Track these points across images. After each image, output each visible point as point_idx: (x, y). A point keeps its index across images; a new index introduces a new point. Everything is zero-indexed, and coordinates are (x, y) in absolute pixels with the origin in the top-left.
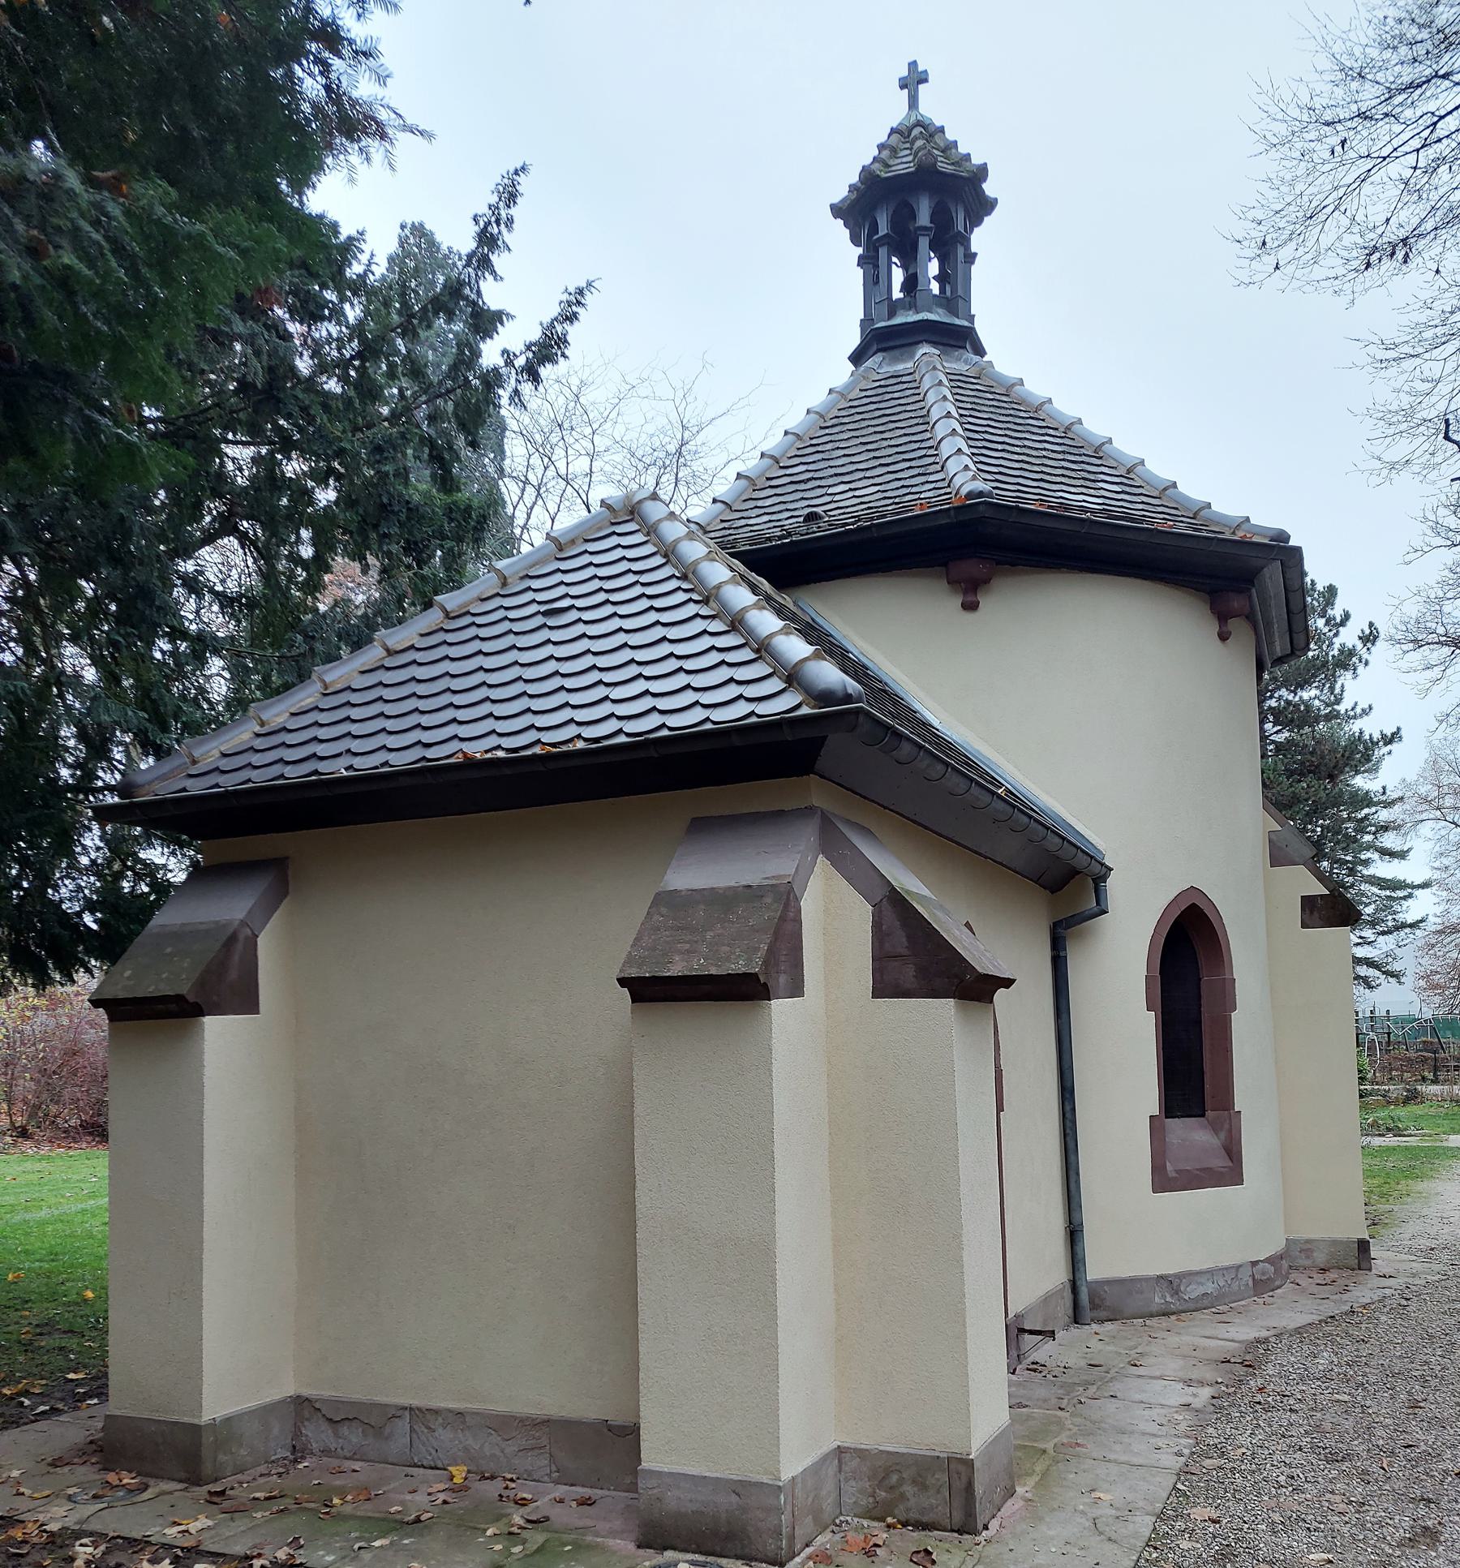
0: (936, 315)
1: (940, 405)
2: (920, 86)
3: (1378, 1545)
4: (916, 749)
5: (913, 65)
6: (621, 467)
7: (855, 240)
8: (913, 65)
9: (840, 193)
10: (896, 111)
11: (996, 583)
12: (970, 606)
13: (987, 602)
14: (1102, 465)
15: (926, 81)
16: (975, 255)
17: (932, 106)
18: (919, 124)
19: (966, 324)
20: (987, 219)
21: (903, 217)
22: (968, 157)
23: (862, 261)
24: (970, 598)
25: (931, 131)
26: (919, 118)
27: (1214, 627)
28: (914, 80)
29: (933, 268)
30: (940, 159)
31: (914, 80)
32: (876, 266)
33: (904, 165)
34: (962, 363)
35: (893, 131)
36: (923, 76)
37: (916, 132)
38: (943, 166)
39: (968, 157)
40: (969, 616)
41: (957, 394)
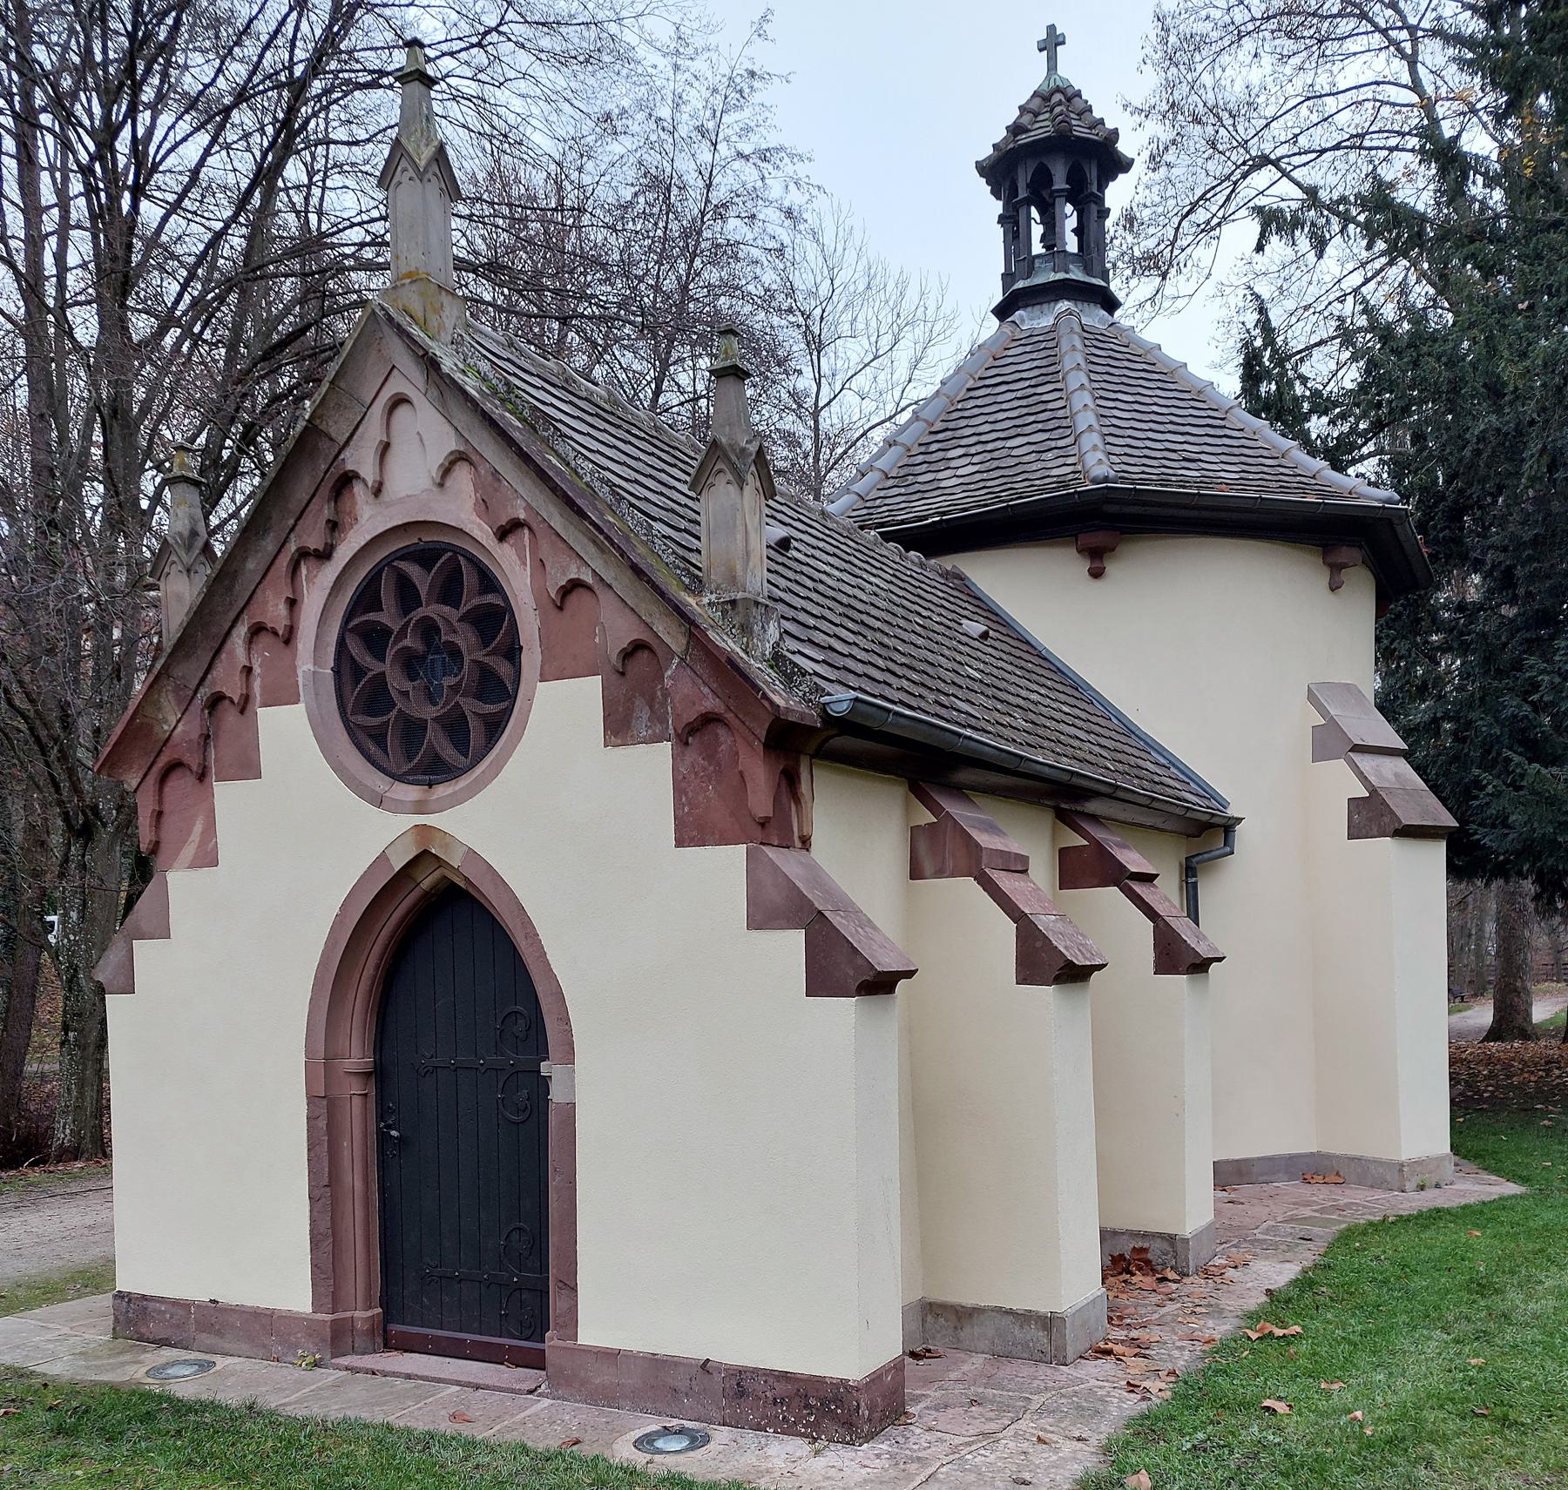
0: (1077, 274)
1: (1073, 356)
2: (1059, 48)
3: (1323, 83)
4: (1018, 760)
5: (1051, 29)
6: (506, 211)
7: (996, 193)
8: (1051, 29)
9: (986, 152)
10: (1034, 76)
11: (1123, 549)
12: (1096, 574)
13: (1113, 568)
14: (1224, 427)
15: (1063, 43)
16: (1109, 210)
17: (1072, 69)
18: (1058, 90)
19: (1103, 284)
20: (1121, 176)
21: (1042, 179)
22: (1101, 122)
23: (1002, 220)
24: (1097, 564)
25: (1071, 96)
26: (1059, 83)
27: (1324, 578)
28: (1052, 43)
29: (1072, 222)
30: (1074, 122)
31: (1052, 43)
32: (1017, 223)
33: (1042, 129)
34: (1094, 317)
35: (1035, 94)
36: (1061, 39)
37: (1058, 97)
38: (1080, 131)
39: (1101, 122)
40: (1097, 584)
41: (1101, 397)
